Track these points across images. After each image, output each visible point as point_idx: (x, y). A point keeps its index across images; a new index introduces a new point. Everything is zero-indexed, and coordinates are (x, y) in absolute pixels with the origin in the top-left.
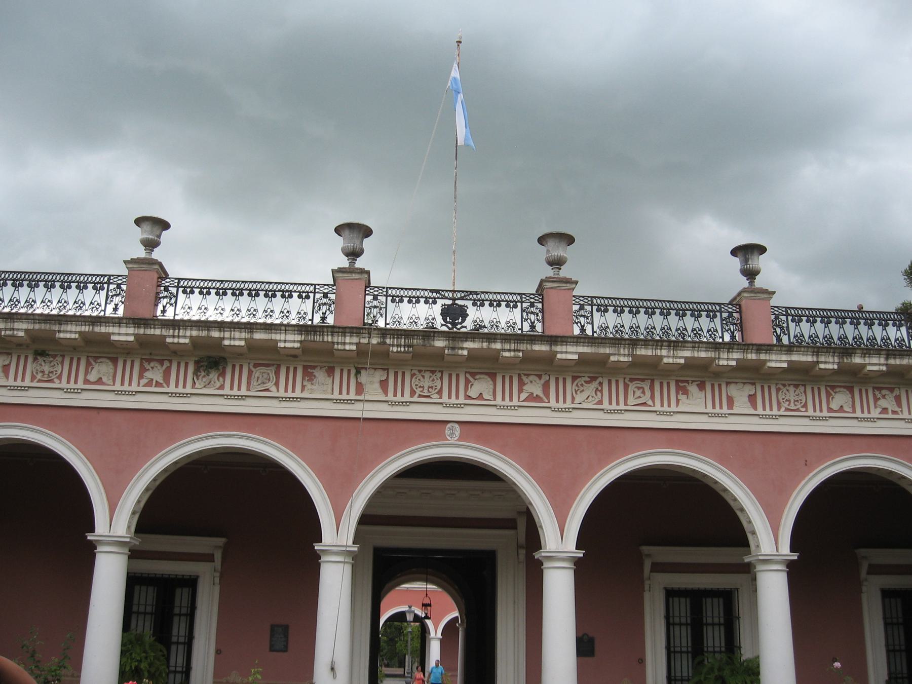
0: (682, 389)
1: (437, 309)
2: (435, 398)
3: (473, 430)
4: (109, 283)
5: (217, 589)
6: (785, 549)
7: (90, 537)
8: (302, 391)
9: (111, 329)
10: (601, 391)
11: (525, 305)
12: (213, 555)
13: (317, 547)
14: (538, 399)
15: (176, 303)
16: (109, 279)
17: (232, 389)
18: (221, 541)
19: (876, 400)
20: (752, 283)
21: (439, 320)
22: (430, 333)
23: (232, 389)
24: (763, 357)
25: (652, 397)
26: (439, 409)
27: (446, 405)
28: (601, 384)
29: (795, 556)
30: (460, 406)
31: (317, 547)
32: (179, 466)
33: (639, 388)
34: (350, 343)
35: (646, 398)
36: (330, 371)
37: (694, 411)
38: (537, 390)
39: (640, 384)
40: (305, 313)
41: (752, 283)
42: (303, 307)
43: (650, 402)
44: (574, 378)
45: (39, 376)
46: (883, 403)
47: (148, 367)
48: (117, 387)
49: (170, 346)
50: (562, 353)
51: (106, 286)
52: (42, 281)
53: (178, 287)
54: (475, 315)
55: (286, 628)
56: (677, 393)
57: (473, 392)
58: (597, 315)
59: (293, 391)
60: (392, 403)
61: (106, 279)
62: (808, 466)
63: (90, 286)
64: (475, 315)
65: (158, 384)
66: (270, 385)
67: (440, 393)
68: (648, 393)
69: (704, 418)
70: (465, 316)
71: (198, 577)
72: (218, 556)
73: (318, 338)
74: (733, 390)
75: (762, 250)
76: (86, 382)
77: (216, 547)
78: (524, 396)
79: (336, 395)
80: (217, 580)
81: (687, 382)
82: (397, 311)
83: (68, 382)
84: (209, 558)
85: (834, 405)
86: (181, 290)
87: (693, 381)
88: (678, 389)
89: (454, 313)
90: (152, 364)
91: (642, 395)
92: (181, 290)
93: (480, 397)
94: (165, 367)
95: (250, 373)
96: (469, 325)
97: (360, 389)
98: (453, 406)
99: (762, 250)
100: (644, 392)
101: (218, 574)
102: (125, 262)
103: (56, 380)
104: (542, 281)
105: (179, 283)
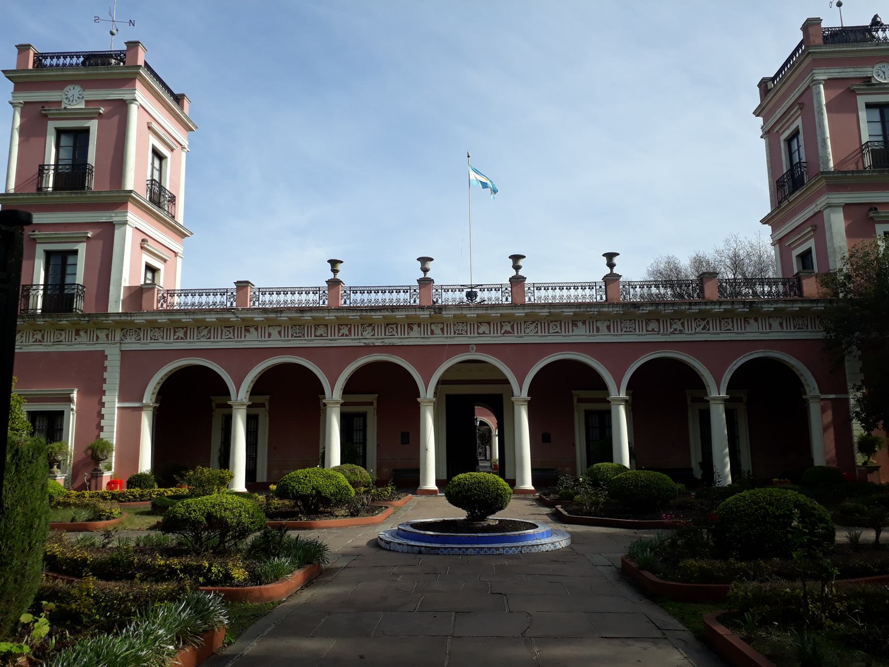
0: (575, 324)
1: (464, 293)
2: (161, 340)
3: (481, 347)
5: (268, 418)
6: (723, 395)
7: (804, 397)
9: (372, 314)
13: (418, 400)
14: (509, 332)
18: (268, 397)
19: (671, 325)
20: (517, 272)
21: (465, 299)
22: (460, 306)
24: (418, 313)
26: (163, 344)
29: (529, 398)
30: (312, 340)
31: (418, 400)
34: (332, 316)
36: (756, 320)
37: (581, 335)
38: (509, 328)
41: (517, 272)
44: (695, 319)
45: (624, 329)
46: (674, 326)
48: (329, 337)
54: (481, 296)
55: (408, 433)
57: (650, 328)
58: (352, 295)
62: (636, 358)
64: (481, 296)
65: (347, 335)
66: (730, 327)
69: (257, 343)
70: (476, 296)
72: (267, 404)
73: (129, 318)
74: (599, 324)
75: (431, 260)
76: (316, 336)
84: (371, 404)
85: (650, 328)
88: (745, 321)
89: (471, 295)
93: (484, 333)
95: (720, 322)
96: (478, 300)
97: (432, 333)
99: (431, 260)
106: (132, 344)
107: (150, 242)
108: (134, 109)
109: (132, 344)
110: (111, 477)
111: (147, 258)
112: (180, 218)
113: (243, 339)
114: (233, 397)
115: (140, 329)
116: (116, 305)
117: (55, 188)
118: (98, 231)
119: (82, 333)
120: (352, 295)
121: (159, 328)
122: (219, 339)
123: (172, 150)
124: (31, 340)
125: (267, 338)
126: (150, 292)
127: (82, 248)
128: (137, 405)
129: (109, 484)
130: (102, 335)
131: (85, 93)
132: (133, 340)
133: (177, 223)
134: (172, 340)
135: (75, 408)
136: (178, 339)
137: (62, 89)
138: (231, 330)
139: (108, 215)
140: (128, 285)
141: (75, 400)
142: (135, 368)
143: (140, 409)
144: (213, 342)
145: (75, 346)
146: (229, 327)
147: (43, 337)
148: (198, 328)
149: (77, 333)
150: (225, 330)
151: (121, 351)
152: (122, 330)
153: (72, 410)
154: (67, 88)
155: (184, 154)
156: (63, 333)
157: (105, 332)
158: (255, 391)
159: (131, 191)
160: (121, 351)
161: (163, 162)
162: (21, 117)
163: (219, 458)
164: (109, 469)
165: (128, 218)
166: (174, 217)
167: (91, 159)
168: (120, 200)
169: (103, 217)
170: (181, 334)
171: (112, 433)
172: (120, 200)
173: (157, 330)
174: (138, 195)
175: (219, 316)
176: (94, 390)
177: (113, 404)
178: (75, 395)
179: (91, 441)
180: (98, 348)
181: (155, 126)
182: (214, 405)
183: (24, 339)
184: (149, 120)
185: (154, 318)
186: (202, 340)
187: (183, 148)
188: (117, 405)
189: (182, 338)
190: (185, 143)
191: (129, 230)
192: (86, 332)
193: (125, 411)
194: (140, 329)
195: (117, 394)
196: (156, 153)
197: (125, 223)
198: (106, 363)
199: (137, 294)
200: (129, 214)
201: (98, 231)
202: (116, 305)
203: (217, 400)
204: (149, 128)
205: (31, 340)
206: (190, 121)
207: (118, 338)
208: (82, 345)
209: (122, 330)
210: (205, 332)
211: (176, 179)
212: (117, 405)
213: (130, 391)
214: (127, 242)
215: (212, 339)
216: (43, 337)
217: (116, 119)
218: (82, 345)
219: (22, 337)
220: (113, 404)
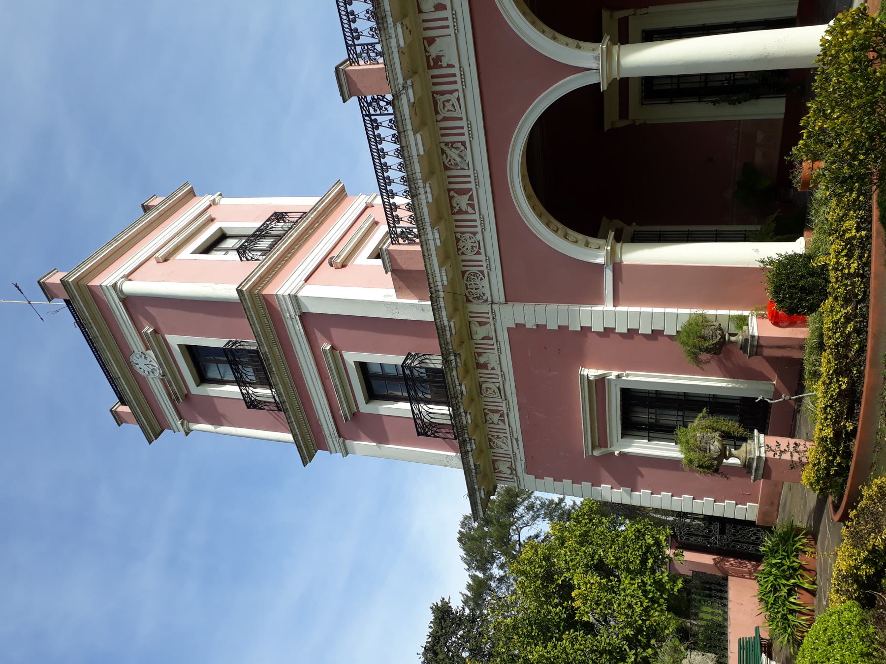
2: (479, 237)
4: (370, 115)
8: (454, 67)
10: (453, 143)
11: (372, 112)
12: (620, 20)
15: (371, 44)
16: (366, 115)
17: (463, 134)
18: (605, 14)
23: (463, 134)
25: (451, 92)
27: (464, 84)
28: (447, 144)
32: (528, 11)
33: (444, 106)
35: (453, 97)
39: (440, 106)
40: (367, 12)
42: (385, 124)
43: (456, 94)
47: (457, 208)
49: (450, 277)
50: (435, 243)
51: (373, 118)
52: (350, 25)
53: (355, 45)
56: (441, 67)
59: (454, 75)
60: (483, 228)
61: (367, 118)
63: (353, 26)
65: (471, 198)
67: (475, 233)
68: (447, 97)
69: (461, 36)
71: (643, 31)
73: (442, 294)
77: (611, 16)
78: (470, 210)
79: (451, 31)
80: (644, 10)
81: (428, 58)
82: (366, 33)
83: (476, 226)
86: (356, 42)
87: (426, 51)
90: (455, 205)
91: (451, 103)
92: (356, 42)
94: (455, 195)
98: (463, 77)
100: (448, 101)
101: (639, 12)
102: (344, 101)
103: (497, 385)
104: (337, 68)
105: (351, 46)
106: (493, 283)
107: (335, 253)
108: (129, 287)
109: (493, 283)
110: (760, 317)
111: (362, 258)
112: (307, 202)
113: (456, 70)
114: (590, 79)
115: (464, 273)
116: (416, 308)
117: (270, 386)
118: (318, 335)
119: (482, 360)
120: (363, 40)
121: (458, 240)
122: (463, 123)
123: (212, 220)
124: (501, 426)
125: (447, 13)
126: (394, 254)
127: (351, 357)
128: (609, 275)
129: (776, 324)
130: (480, 332)
131: (136, 351)
132: (485, 282)
133: (314, 208)
134: (476, 217)
135: (614, 374)
136: (472, 206)
137: (144, 378)
138: (441, 99)
139: (290, 323)
140: (392, 291)
141: (601, 372)
142: (533, 276)
143: (618, 268)
144: (471, 136)
145: (505, 369)
146: (435, 103)
147: (497, 411)
148: (446, 168)
149: (485, 366)
150: (443, 114)
151: (507, 301)
152: (468, 301)
153: (618, 377)
154: (141, 372)
155: (224, 201)
156: (484, 386)
157: (475, 327)
158: (585, 31)
159: (239, 291)
160: (507, 301)
161: (229, 232)
162: (198, 423)
163: (733, 103)
164: (742, 321)
165: (286, 294)
166: (305, 213)
167: (219, 343)
168: (255, 304)
169: (295, 330)
170: (462, 201)
171: (673, 316)
172: (255, 304)
173: (461, 244)
174: (247, 280)
175: (409, 127)
176: (575, 343)
177: (604, 313)
178: (592, 373)
179: (680, 351)
180: (504, 337)
181: (160, 254)
182: (622, 124)
183: (501, 435)
184: (153, 261)
185: (433, 252)
186: (469, 159)
187: (214, 203)
188: (609, 307)
189: (471, 198)
190: (206, 201)
191: (309, 291)
192: (480, 354)
193: (621, 293)
194: (464, 273)
195: (576, 307)
196: (208, 248)
197: (295, 298)
198: (530, 325)
199: (404, 278)
200: (280, 293)
201: (318, 335)
202: (416, 308)
203: (611, 117)
204: (166, 260)
205: (501, 426)
206: (174, 194)
207: (486, 308)
208: (501, 361)
209: (468, 301)
210: (453, 154)
211: (242, 213)
212: (609, 307)
213: (584, 284)
214: (329, 292)
215: (465, 138)
216: (497, 411)
217: (152, 310)
218: (501, 361)
219: (498, 437)
220: (604, 313)
